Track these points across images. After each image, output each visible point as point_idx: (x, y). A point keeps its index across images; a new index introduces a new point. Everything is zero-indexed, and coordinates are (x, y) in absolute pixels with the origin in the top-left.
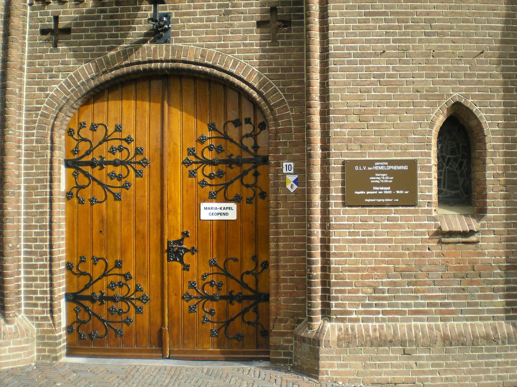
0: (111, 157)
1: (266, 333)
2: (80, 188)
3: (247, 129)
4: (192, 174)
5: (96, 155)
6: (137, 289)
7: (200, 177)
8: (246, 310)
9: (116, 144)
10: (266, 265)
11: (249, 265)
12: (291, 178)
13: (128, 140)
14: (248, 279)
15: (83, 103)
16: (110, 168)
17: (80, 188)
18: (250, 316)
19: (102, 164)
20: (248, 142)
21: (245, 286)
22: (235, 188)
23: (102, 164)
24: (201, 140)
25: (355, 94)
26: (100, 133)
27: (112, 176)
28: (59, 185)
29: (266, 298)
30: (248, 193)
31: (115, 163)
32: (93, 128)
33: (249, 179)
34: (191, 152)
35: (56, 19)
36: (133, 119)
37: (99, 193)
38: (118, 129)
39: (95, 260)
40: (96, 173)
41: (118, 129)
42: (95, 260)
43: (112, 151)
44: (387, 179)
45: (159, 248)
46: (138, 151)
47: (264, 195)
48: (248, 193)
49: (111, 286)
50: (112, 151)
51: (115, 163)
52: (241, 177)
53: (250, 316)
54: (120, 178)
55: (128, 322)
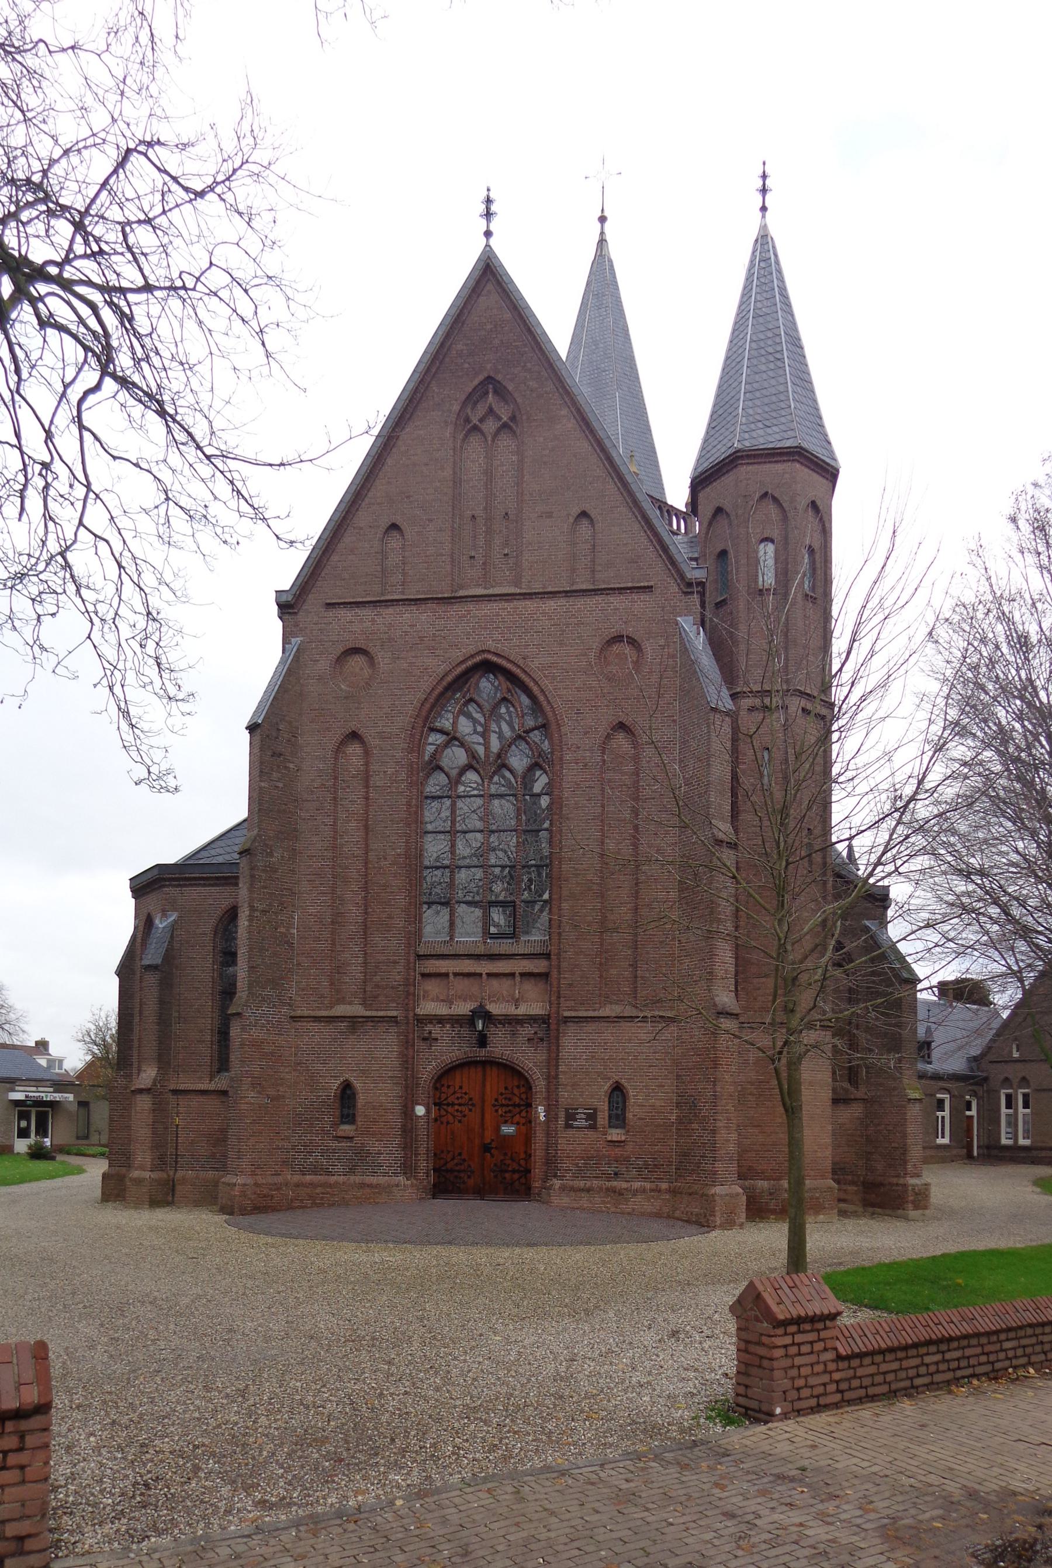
0: (456, 1102)
1: (529, 1188)
2: (441, 1116)
3: (523, 1090)
4: (497, 1111)
5: (450, 1100)
6: (469, 1166)
7: (500, 1112)
8: (520, 1177)
9: (459, 1095)
10: (530, 1156)
11: (522, 1156)
12: (543, 1114)
13: (466, 1094)
14: (522, 1162)
15: (22, 297)
16: (456, 1107)
17: (441, 1116)
18: (523, 1180)
19: (453, 1104)
20: (524, 1096)
21: (520, 1165)
22: (517, 1118)
23: (453, 1104)
24: (502, 1094)
25: (657, 1013)
26: (451, 1090)
27: (457, 1110)
28: (804, 1332)
29: (530, 1171)
30: (523, 1121)
31: (460, 1105)
32: (449, 1087)
33: (524, 1114)
34: (496, 1100)
35: (430, 1033)
36: (369, 599)
37: (451, 1119)
38: (461, 1088)
39: (449, 1152)
40: (450, 1109)
41: (461, 1088)
42: (449, 1152)
43: (458, 1098)
44: (584, 1116)
45: (376, 431)
46: (471, 1099)
47: (530, 1122)
48: (523, 1121)
49: (457, 1165)
50: (458, 1098)
51: (460, 1105)
52: (520, 1113)
53: (523, 1180)
54: (461, 1112)
55: (464, 1183)
